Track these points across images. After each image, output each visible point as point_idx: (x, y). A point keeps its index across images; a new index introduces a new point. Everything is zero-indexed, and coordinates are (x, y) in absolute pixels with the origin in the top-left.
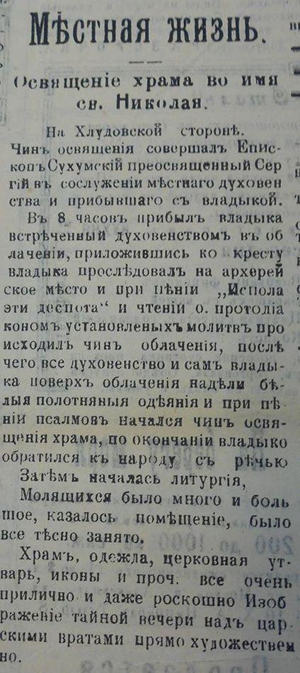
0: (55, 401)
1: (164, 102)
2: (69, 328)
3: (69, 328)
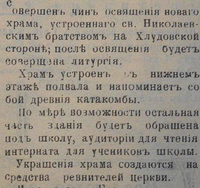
0: (60, 139)
1: (129, 155)
2: (63, 75)
3: (63, 75)
